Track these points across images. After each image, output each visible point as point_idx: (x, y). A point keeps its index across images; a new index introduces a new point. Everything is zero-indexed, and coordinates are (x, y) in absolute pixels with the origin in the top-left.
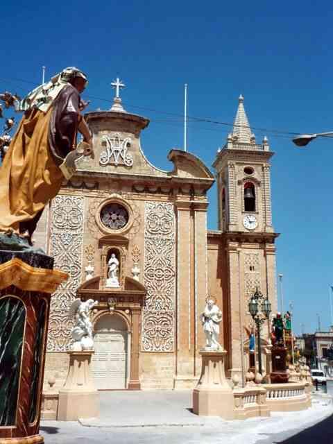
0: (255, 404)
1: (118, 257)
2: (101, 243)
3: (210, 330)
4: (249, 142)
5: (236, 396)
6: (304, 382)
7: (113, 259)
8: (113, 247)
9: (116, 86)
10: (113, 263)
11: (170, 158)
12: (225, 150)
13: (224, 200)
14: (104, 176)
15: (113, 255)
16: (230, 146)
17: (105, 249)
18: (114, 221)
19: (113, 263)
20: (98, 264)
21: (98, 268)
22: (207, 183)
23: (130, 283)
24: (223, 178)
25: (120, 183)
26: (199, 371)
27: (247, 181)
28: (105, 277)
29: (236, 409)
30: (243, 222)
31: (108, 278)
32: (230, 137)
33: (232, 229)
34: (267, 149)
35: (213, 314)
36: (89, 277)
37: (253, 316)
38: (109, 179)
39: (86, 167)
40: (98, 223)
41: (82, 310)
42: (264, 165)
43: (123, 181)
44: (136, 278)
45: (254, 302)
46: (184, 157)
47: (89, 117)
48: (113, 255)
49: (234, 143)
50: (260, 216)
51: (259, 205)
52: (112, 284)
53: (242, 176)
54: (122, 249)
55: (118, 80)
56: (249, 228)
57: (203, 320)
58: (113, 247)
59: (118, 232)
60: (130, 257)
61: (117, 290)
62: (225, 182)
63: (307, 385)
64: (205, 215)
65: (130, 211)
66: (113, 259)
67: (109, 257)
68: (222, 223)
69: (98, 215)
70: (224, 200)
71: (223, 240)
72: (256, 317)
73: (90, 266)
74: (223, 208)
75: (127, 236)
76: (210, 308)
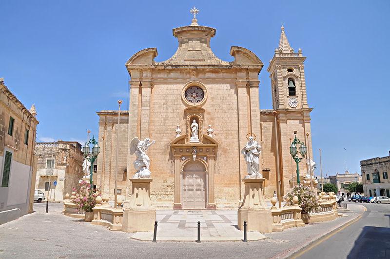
0: (292, 220)
1: (197, 122)
2: (186, 112)
3: (250, 161)
4: (290, 52)
5: (274, 214)
6: (332, 202)
7: (194, 124)
8: (194, 116)
9: (193, 12)
10: (194, 126)
11: (231, 54)
12: (275, 59)
13: (275, 91)
14: (186, 67)
15: (194, 121)
16: (277, 56)
17: (188, 118)
18: (194, 97)
19: (194, 126)
20: (184, 127)
21: (185, 130)
22: (257, 67)
23: (206, 139)
24: (274, 76)
25: (197, 70)
26: (243, 195)
27: (290, 77)
28: (189, 135)
29: (274, 225)
30: (287, 102)
31: (191, 136)
32: (277, 50)
33: (281, 107)
34: (301, 56)
35: (253, 148)
36: (178, 136)
37: (294, 156)
38: (190, 69)
39: (175, 63)
40: (183, 99)
41: (139, 147)
42: (300, 66)
43: (199, 70)
44: (210, 135)
45: (293, 146)
46: (241, 51)
47: (176, 31)
48: (194, 121)
49: (279, 54)
50: (299, 99)
51: (298, 91)
52: (194, 140)
53: (285, 73)
54: (200, 117)
55: (195, 8)
56: (292, 106)
57: (245, 154)
58: (194, 116)
59: (197, 104)
60: (206, 122)
61: (197, 144)
62: (276, 80)
63: (334, 204)
64: (257, 90)
65: (205, 91)
66: (194, 124)
67: (191, 122)
68: (275, 106)
69: (183, 94)
70: (275, 91)
71: (274, 115)
72: (296, 157)
73: (179, 129)
74: (276, 95)
75: (203, 107)
76: (250, 143)
